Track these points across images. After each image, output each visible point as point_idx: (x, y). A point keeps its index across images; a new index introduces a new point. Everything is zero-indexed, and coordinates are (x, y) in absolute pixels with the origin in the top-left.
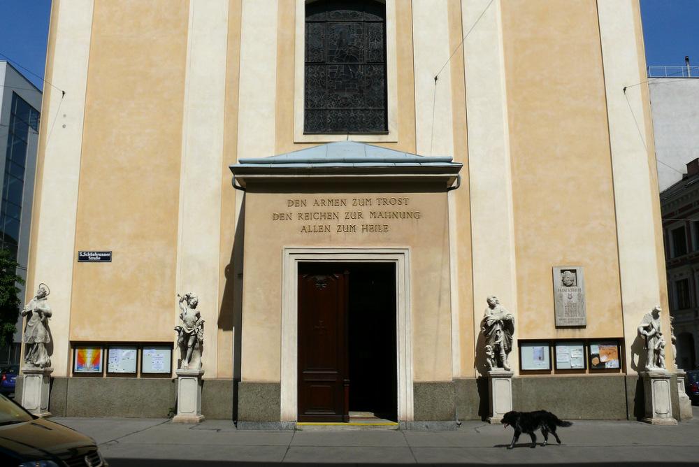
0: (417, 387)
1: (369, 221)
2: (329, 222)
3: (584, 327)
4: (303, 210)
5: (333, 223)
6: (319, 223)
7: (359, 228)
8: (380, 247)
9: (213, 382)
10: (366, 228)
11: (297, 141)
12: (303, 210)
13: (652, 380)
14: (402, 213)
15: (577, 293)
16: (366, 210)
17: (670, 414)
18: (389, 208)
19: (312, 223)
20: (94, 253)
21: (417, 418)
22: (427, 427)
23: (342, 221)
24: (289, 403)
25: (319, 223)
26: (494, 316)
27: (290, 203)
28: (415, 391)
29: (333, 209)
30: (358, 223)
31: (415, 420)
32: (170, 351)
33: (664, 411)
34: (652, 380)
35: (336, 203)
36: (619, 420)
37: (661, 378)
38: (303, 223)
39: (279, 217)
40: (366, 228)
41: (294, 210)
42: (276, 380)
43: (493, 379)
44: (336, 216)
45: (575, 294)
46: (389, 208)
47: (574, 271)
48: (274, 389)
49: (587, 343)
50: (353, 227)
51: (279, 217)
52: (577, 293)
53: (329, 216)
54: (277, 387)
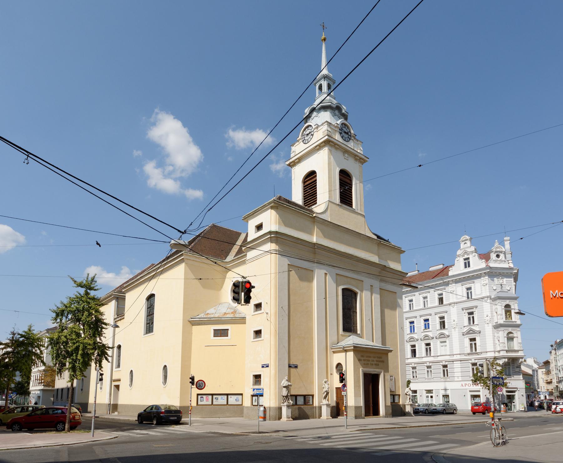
16: (375, 359)
19: (366, 362)
53: (369, 361)
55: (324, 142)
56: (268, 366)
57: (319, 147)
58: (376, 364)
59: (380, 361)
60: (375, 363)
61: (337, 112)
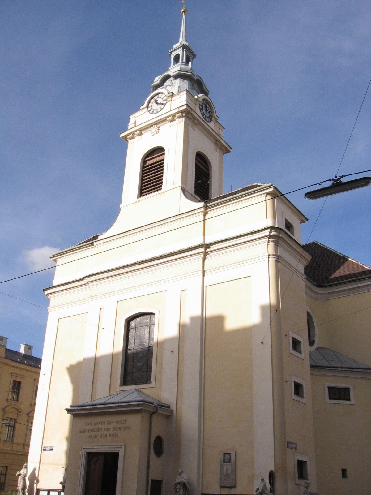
3: (235, 487)
5: (99, 433)
12: (90, 427)
15: (231, 467)
16: (111, 427)
19: (93, 434)
27: (87, 425)
29: (99, 427)
35: (101, 424)
39: (82, 431)
41: (87, 428)
45: (229, 467)
50: (106, 435)
51: (82, 431)
53: (99, 430)
55: (182, 112)
56: (51, 450)
57: (173, 118)
58: (112, 436)
59: (120, 429)
60: (111, 432)
61: (196, 86)
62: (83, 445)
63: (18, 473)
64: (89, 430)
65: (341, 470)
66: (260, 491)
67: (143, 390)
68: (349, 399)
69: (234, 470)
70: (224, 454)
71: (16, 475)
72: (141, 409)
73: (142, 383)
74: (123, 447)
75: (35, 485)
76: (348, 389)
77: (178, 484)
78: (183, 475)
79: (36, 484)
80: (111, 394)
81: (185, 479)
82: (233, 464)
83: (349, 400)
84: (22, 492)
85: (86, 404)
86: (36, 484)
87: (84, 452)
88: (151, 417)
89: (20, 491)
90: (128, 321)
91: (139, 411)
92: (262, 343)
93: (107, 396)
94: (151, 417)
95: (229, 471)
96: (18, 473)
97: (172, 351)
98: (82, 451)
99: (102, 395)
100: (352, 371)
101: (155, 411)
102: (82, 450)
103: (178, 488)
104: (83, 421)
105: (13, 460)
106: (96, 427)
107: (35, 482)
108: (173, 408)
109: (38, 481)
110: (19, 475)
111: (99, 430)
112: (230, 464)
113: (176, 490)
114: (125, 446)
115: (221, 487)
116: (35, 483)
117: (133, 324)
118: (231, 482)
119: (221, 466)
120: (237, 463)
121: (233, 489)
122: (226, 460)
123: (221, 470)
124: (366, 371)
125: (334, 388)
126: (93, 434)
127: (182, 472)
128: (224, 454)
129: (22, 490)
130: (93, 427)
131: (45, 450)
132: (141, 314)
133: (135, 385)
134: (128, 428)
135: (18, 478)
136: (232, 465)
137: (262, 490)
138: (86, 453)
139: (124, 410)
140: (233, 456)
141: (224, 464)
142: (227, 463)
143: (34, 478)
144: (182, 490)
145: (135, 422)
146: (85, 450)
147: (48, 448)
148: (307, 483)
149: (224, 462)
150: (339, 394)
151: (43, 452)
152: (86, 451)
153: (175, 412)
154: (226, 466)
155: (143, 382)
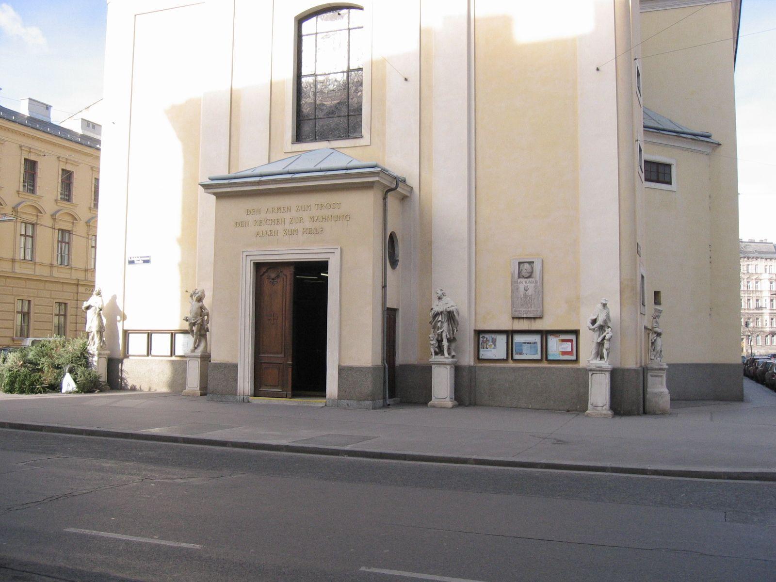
0: (341, 370)
1: (308, 224)
2: (278, 227)
3: (541, 318)
4: (258, 217)
5: (279, 228)
6: (269, 228)
7: (301, 230)
8: (315, 248)
9: (218, 366)
10: (305, 231)
11: (286, 152)
12: (258, 217)
13: (590, 373)
14: (330, 217)
15: (534, 284)
16: (305, 215)
17: (607, 406)
18: (325, 212)
19: (265, 228)
20: (138, 257)
21: (340, 397)
22: (348, 405)
23: (287, 226)
24: (245, 382)
25: (269, 228)
26: (438, 307)
27: (248, 212)
28: (339, 374)
29: (280, 216)
30: (300, 227)
31: (338, 399)
32: (401, 359)
33: (600, 404)
34: (590, 373)
35: (282, 210)
36: (568, 411)
37: (599, 371)
38: (257, 228)
39: (241, 224)
40: (305, 231)
41: (251, 218)
42: (234, 362)
43: (433, 366)
44: (283, 221)
45: (531, 286)
46: (325, 212)
47: (530, 263)
48: (233, 368)
49: (545, 334)
50: (296, 231)
51: (241, 224)
52: (534, 284)
53: (277, 222)
54: (235, 367)
59: (327, 219)
62: (244, 250)
63: (86, 304)
64: (256, 221)
65: (654, 293)
66: (602, 324)
67: (345, 150)
68: (669, 183)
69: (541, 290)
70: (520, 263)
71: (82, 308)
72: (373, 182)
73: (338, 137)
74: (338, 252)
75: (120, 326)
76: (669, 166)
77: (437, 315)
78: (445, 299)
79: (121, 322)
80: (271, 161)
81: (452, 306)
82: (538, 280)
83: (670, 183)
84: (99, 336)
85: (238, 174)
86: (121, 322)
87: (248, 262)
88: (385, 198)
89: (94, 335)
90: (300, 20)
91: (368, 186)
92: (598, 69)
93: (264, 163)
94: (385, 198)
95: (530, 292)
96: (86, 304)
97: (406, 79)
98: (244, 260)
99: (254, 159)
100: (679, 137)
101: (394, 186)
102: (245, 257)
103: (440, 321)
104: (238, 208)
105: (13, 287)
106: (270, 216)
107: (119, 318)
108: (413, 182)
109: (124, 318)
110: (88, 308)
111: (277, 222)
112: (533, 280)
113: (435, 324)
114: (341, 250)
115: (513, 318)
116: (119, 321)
117: (305, 25)
118: (533, 309)
119: (513, 283)
120: (546, 278)
121: (538, 321)
122: (524, 273)
123: (515, 290)
124: (696, 138)
125: (654, 162)
126: (265, 228)
127: (444, 294)
128: (520, 263)
129: (97, 333)
130: (263, 216)
131: (132, 262)
132: (337, 7)
133: (327, 140)
134: (346, 217)
135: (86, 313)
136: (536, 282)
137: (605, 321)
138: (254, 263)
139: (355, 183)
140: (537, 267)
141: (520, 280)
142: (525, 278)
143: (113, 313)
144: (445, 325)
145: (363, 206)
146: (249, 258)
147: (138, 259)
148: (657, 309)
149: (520, 276)
150: (658, 173)
151: (130, 267)
152: (251, 260)
153: (416, 190)
154: (523, 284)
155: (340, 136)
